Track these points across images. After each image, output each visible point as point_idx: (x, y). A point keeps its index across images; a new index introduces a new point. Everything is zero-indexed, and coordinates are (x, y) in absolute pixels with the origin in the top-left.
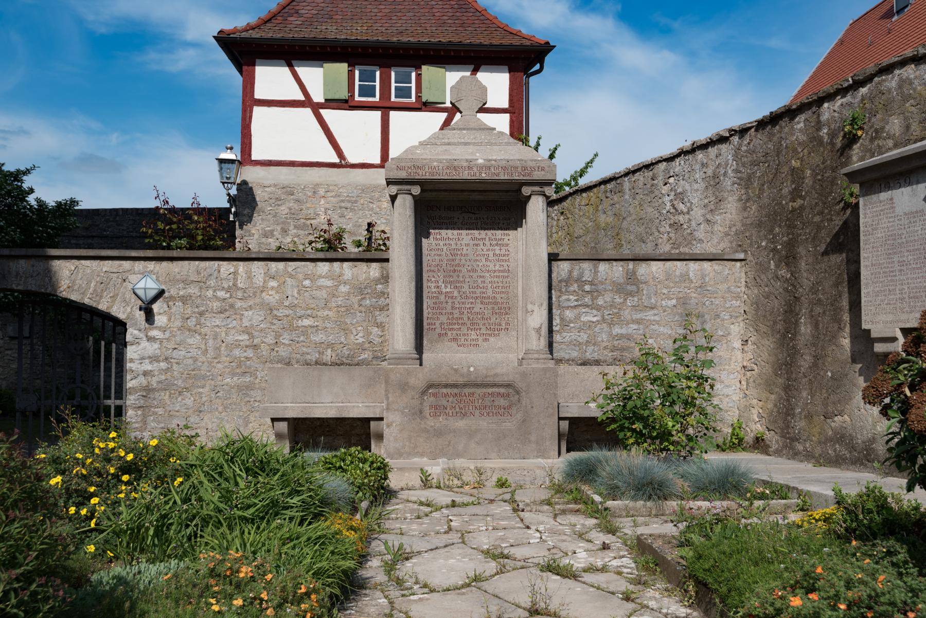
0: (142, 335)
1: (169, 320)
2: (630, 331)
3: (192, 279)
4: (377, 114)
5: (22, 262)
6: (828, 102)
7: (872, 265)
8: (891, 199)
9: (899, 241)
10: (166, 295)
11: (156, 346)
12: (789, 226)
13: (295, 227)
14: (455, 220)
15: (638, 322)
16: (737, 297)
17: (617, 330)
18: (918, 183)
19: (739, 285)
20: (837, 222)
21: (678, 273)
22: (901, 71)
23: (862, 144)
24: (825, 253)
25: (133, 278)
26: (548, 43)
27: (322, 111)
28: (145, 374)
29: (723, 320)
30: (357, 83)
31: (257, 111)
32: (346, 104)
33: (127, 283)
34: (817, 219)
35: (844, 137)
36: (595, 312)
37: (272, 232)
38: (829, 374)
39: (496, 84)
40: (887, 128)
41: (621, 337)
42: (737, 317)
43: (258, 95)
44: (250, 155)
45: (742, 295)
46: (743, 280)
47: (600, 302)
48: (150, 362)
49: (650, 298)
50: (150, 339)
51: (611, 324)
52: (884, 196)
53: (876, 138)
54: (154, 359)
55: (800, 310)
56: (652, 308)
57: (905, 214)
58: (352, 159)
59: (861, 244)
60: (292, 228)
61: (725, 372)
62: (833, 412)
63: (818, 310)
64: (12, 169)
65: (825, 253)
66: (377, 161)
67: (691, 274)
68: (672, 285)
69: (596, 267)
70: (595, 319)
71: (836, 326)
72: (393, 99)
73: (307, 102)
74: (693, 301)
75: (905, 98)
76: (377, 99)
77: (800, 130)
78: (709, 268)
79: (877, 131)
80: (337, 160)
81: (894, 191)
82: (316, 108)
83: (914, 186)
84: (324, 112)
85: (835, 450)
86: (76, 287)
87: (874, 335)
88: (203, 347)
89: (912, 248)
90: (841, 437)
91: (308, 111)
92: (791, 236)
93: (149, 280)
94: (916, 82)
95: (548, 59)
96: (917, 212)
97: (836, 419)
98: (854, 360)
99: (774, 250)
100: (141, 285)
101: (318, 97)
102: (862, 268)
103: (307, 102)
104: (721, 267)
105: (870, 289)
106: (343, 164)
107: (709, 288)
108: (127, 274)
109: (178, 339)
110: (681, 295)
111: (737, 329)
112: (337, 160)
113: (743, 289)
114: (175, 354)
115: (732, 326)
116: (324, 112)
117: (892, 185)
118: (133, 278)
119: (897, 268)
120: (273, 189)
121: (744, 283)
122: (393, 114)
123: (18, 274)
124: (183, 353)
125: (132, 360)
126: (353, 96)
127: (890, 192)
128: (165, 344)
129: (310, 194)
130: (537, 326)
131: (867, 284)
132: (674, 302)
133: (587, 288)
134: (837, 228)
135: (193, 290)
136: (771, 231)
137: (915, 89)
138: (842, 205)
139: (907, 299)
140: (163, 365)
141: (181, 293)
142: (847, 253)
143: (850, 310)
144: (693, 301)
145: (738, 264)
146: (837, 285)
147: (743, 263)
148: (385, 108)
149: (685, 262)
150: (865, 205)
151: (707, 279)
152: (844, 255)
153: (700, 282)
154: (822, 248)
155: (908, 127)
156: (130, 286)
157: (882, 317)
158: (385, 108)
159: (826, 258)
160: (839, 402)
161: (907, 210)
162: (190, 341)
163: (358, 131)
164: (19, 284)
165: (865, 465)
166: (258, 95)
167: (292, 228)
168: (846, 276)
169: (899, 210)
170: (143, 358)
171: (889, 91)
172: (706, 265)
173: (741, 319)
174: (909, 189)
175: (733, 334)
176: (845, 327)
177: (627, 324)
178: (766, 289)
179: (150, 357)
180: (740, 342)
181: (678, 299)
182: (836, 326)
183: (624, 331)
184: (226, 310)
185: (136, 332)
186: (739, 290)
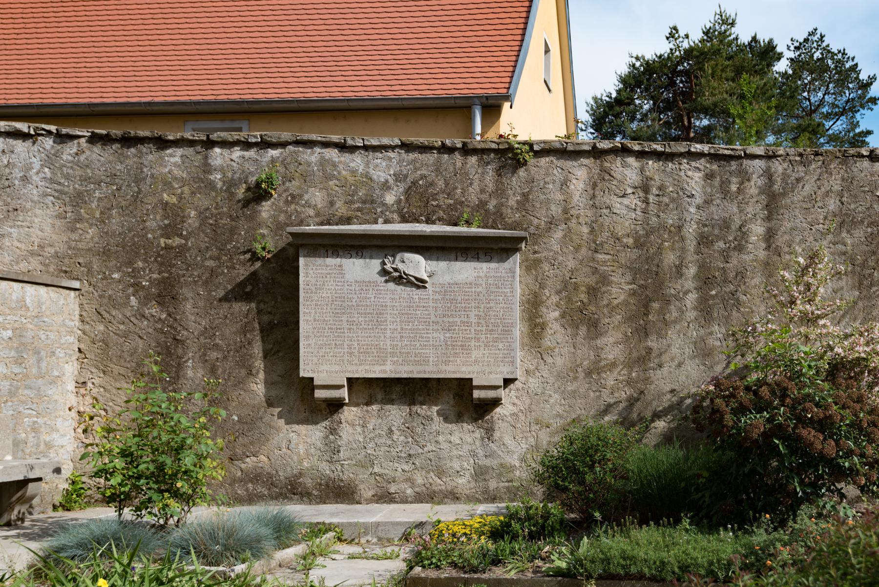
6: (221, 148)
7: (315, 320)
9: (350, 304)
12: (162, 264)
16: (71, 332)
18: (371, 258)
19: (73, 318)
20: (241, 272)
21: (14, 298)
22: (323, 150)
23: (273, 204)
24: (225, 299)
29: (58, 358)
34: (210, 263)
35: (248, 189)
38: (236, 418)
40: (306, 197)
42: (71, 355)
45: (75, 329)
46: (77, 313)
52: (331, 261)
53: (292, 203)
55: (185, 353)
57: (356, 281)
59: (301, 300)
61: (60, 419)
62: (244, 453)
63: (214, 355)
64: (750, 39)
65: (225, 299)
67: (28, 301)
68: (7, 311)
71: (244, 372)
74: (30, 334)
75: (328, 177)
77: (175, 164)
78: (46, 295)
79: (293, 197)
81: (344, 260)
83: (368, 260)
85: (247, 490)
87: (316, 382)
89: (363, 311)
90: (255, 477)
92: (166, 275)
94: (341, 166)
96: (370, 282)
97: (248, 460)
98: (270, 403)
99: (137, 286)
102: (301, 322)
104: (56, 295)
105: (312, 341)
107: (46, 319)
110: (16, 325)
111: (70, 369)
113: (77, 324)
115: (66, 365)
117: (341, 253)
121: (77, 317)
127: (339, 260)
132: (9, 333)
134: (242, 278)
136: (130, 263)
137: (339, 173)
138: (248, 256)
139: (356, 353)
142: (258, 303)
143: (265, 357)
144: (30, 334)
145: (72, 293)
146: (244, 331)
147: (77, 293)
149: (21, 284)
150: (306, 265)
151: (44, 307)
152: (253, 305)
153: (36, 311)
154: (221, 293)
155: (332, 203)
157: (325, 367)
159: (226, 305)
160: (252, 443)
165: (291, 499)
168: (257, 326)
171: (309, 164)
172: (42, 290)
173: (74, 358)
174: (361, 261)
175: (67, 374)
176: (258, 372)
178: (122, 327)
180: (74, 384)
181: (14, 330)
182: (244, 372)
186: (72, 324)
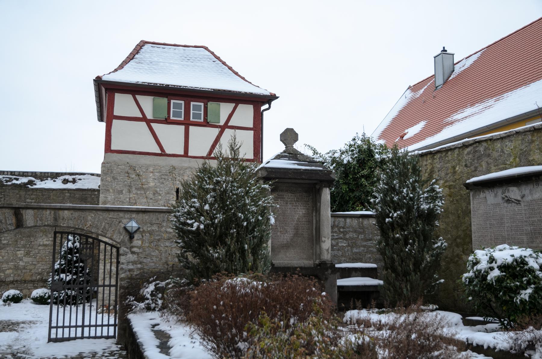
0: (128, 250)
1: (142, 243)
2: (360, 251)
3: (154, 222)
4: (183, 127)
5: (66, 212)
8: (486, 198)
10: (141, 230)
11: (135, 256)
13: (136, 189)
14: (285, 196)
15: (364, 246)
17: (355, 250)
25: (124, 221)
26: (275, 95)
27: (152, 124)
28: (130, 270)
30: (172, 110)
31: (115, 121)
32: (167, 121)
33: (121, 224)
36: (345, 241)
37: (122, 191)
39: (244, 115)
41: (356, 253)
43: (115, 113)
44: (110, 147)
47: (347, 236)
48: (133, 265)
49: (369, 235)
50: (133, 253)
51: (352, 247)
54: (134, 263)
56: (370, 240)
58: (168, 151)
60: (134, 189)
66: (182, 153)
69: (345, 220)
70: (345, 245)
72: (191, 119)
73: (144, 119)
76: (182, 119)
80: (160, 152)
82: (149, 122)
84: (153, 125)
86: (94, 226)
88: (159, 257)
91: (144, 124)
93: (134, 222)
95: (273, 103)
100: (129, 224)
101: (149, 116)
103: (144, 119)
105: (477, 234)
106: (163, 154)
108: (121, 219)
109: (147, 253)
112: (160, 152)
114: (145, 261)
116: (153, 125)
118: (124, 221)
119: (488, 226)
120: (124, 167)
122: (191, 128)
123: (63, 218)
124: (149, 260)
125: (123, 264)
126: (169, 117)
128: (140, 255)
129: (144, 170)
130: (327, 248)
131: (475, 232)
133: (342, 230)
135: (155, 228)
140: (139, 266)
141: (149, 229)
148: (187, 124)
156: (123, 226)
158: (187, 124)
161: (493, 203)
162: (153, 254)
163: (172, 137)
164: (64, 224)
166: (115, 113)
167: (134, 189)
169: (489, 202)
170: (129, 262)
177: (359, 247)
179: (132, 262)
183: (357, 251)
184: (171, 238)
185: (125, 249)
